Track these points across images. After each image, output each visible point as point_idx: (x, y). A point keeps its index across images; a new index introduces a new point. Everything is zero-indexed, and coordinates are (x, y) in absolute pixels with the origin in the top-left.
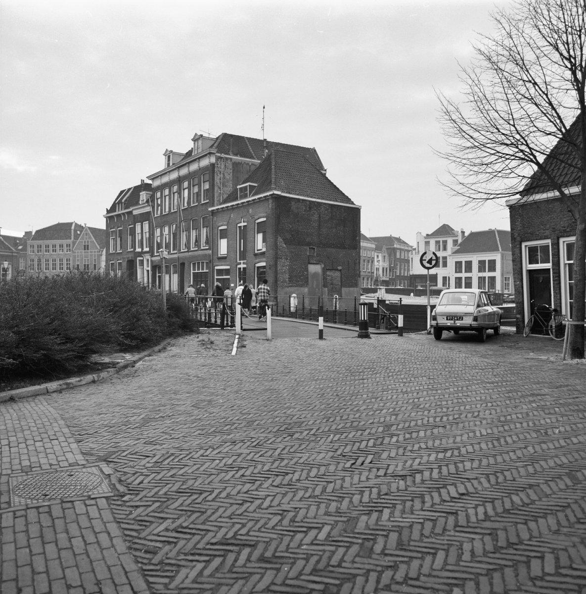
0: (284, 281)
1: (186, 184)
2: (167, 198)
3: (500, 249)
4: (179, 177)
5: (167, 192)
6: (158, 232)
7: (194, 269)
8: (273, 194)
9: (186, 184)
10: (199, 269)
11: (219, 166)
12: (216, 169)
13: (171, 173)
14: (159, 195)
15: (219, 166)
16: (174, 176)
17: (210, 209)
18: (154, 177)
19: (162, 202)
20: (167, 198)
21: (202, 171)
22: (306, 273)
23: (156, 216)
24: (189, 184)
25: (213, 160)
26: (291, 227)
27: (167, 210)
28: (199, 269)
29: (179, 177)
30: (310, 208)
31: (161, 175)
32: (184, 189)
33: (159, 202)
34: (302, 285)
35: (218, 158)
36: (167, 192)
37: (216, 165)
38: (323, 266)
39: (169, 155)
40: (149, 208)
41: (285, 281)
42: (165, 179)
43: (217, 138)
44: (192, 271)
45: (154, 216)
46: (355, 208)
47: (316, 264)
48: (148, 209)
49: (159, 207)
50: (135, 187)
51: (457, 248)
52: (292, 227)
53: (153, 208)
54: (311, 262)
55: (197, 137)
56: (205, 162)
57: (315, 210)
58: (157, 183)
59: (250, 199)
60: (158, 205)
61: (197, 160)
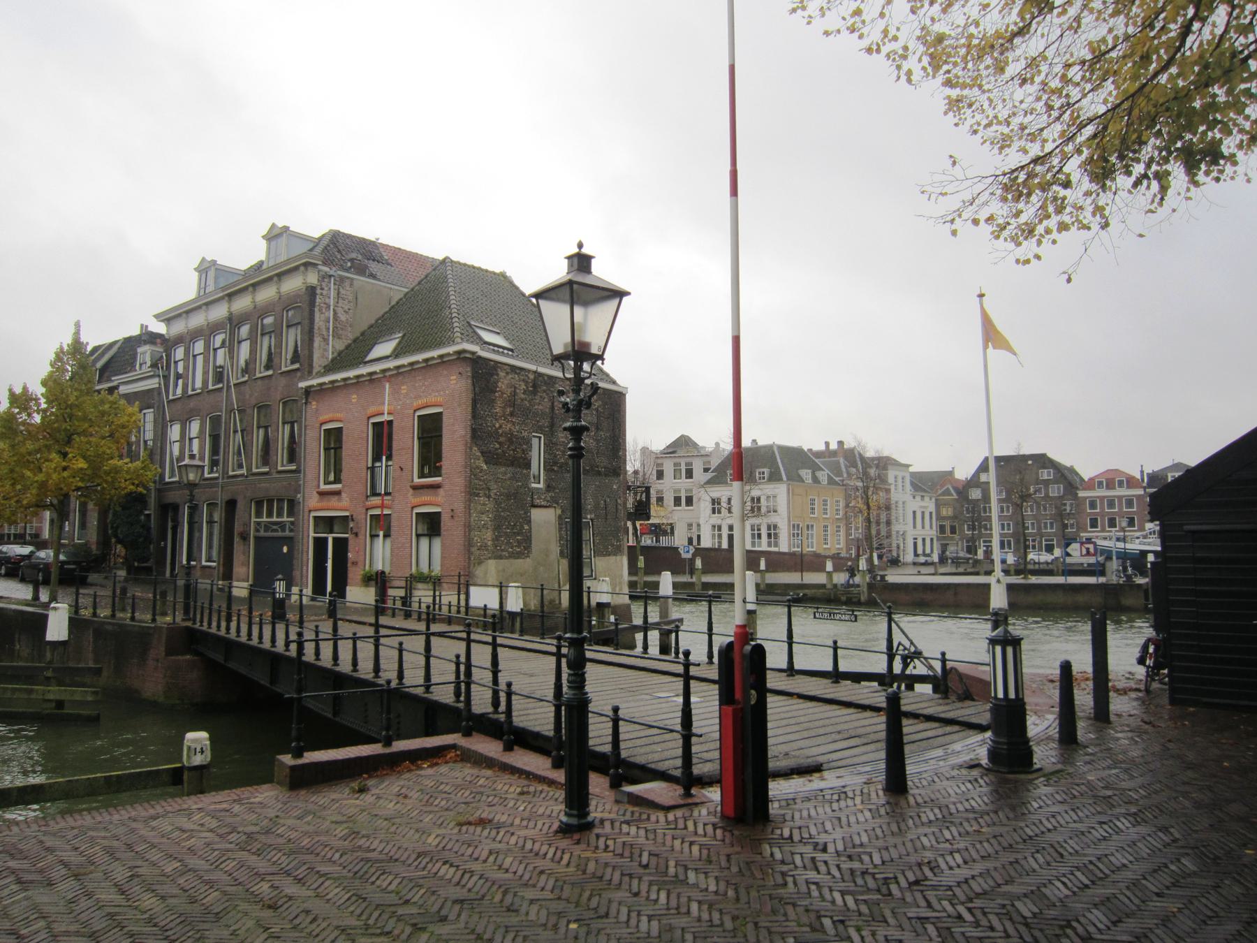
0: (484, 547)
1: (245, 330)
2: (200, 359)
3: (784, 478)
4: (231, 314)
5: (199, 347)
6: (175, 432)
7: (259, 514)
8: (464, 351)
9: (245, 330)
10: (270, 514)
11: (325, 292)
12: (318, 300)
13: (190, 315)
14: (179, 353)
15: (325, 292)
16: (219, 312)
17: (302, 385)
18: (168, 317)
19: (186, 368)
20: (200, 359)
21: (287, 303)
22: (526, 527)
23: (171, 397)
24: (207, 346)
25: (312, 278)
26: (497, 425)
27: (199, 384)
28: (270, 514)
29: (231, 314)
30: (534, 386)
31: (187, 312)
32: (239, 342)
33: (180, 370)
34: (518, 553)
35: (325, 277)
36: (199, 347)
37: (318, 291)
38: (559, 512)
39: (206, 269)
40: (156, 380)
41: (486, 546)
42: (198, 320)
43: (320, 239)
44: (253, 519)
45: (167, 397)
46: (617, 392)
47: (546, 507)
48: (153, 383)
49: (180, 382)
50: (128, 340)
51: (709, 475)
52: (501, 427)
53: (166, 378)
54: (537, 502)
55: (275, 232)
56: (293, 284)
57: (544, 391)
58: (179, 328)
59: (314, 382)
60: (178, 376)
61: (204, 307)
